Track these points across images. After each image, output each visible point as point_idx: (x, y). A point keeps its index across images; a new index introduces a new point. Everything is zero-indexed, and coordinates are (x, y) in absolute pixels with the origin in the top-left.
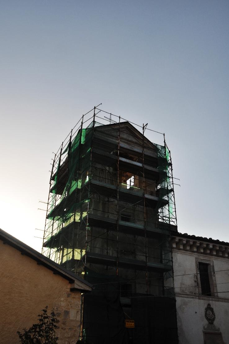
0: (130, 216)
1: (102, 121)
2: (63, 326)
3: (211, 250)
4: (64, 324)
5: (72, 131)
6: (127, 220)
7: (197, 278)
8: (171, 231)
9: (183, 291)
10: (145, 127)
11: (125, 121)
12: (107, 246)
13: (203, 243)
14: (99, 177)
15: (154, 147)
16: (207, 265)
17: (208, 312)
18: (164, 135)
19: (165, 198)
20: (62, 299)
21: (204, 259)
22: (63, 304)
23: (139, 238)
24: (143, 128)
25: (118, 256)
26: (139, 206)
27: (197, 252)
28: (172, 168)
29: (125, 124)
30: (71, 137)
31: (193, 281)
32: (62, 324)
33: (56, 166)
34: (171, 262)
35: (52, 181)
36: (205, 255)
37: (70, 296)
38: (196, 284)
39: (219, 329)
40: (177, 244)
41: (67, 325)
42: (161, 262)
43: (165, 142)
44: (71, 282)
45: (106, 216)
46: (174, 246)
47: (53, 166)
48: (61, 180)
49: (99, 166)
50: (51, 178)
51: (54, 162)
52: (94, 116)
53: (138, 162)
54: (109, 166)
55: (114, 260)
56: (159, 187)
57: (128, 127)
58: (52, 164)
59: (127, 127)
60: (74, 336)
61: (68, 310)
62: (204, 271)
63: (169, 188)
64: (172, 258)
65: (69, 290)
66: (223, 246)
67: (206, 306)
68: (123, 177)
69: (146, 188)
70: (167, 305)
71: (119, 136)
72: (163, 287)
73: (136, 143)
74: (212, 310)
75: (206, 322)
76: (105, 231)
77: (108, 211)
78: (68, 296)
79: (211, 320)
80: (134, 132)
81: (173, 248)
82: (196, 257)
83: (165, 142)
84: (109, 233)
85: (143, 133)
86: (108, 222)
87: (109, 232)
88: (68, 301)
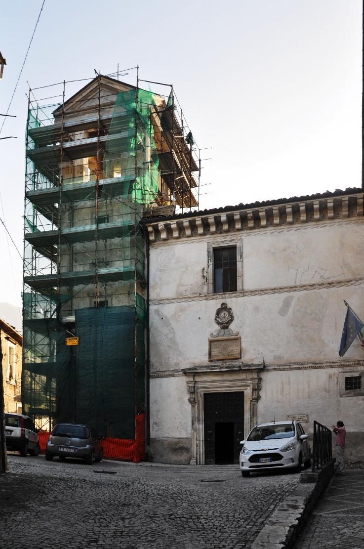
21: (222, 240)
39: (238, 333)
43: (64, 92)
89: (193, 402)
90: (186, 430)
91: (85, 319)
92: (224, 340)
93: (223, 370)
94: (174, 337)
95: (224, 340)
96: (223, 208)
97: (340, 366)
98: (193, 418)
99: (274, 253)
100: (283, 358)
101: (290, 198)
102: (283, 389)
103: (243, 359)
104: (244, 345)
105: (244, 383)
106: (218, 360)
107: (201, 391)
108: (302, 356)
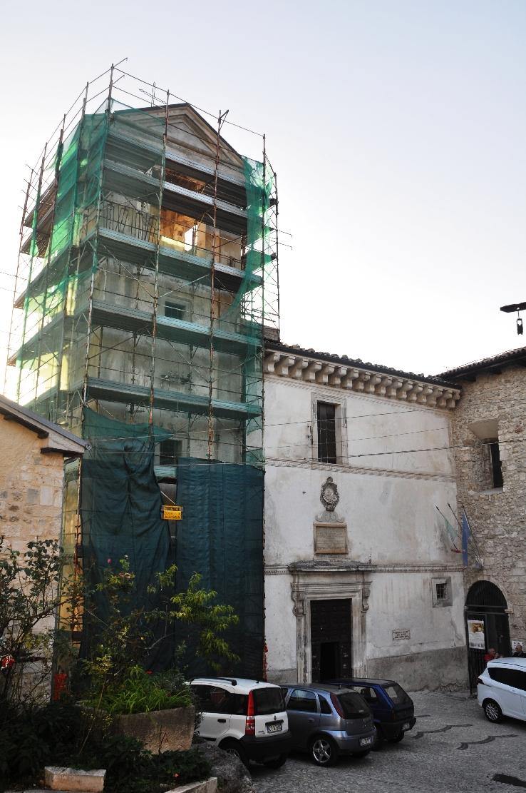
0: (183, 307)
1: (131, 98)
2: (26, 516)
3: (343, 378)
4: (29, 513)
5: (64, 119)
6: (179, 316)
7: (311, 432)
8: (265, 339)
9: (283, 454)
10: (223, 118)
11: (183, 102)
12: (134, 367)
13: (286, 357)
14: (118, 222)
15: (242, 165)
16: (334, 406)
17: (326, 492)
18: (264, 138)
19: (258, 272)
20: (24, 468)
21: (329, 395)
22: (25, 477)
23: (201, 351)
24: (220, 120)
25: (152, 386)
26: (204, 286)
27: (317, 381)
28: (277, 210)
29: (182, 109)
30: (62, 132)
31: (304, 437)
32: (25, 514)
33: (34, 194)
34: (261, 401)
35: (25, 228)
36: (330, 388)
37: (41, 462)
38: (310, 442)
39: (343, 519)
40: (277, 365)
41: (34, 514)
42: (243, 400)
43: (264, 153)
44: (43, 435)
45: (133, 306)
46: (271, 368)
47: (28, 196)
48: (41, 225)
49: (120, 199)
50: (22, 223)
51: (30, 185)
52: (111, 86)
53: (207, 193)
54: (142, 201)
55: (145, 395)
56: (247, 249)
57: (187, 116)
58: (26, 192)
59: (186, 115)
60: (50, 534)
61: (36, 489)
62: (327, 416)
63: (268, 253)
64: (263, 392)
65: (37, 451)
66: (368, 372)
67: (324, 481)
68: (176, 226)
69: (220, 251)
70: (250, 480)
71: (166, 134)
72: (244, 447)
73: (203, 153)
74: (334, 487)
75: (321, 508)
76: (131, 335)
77: (137, 294)
78: (37, 462)
79: (330, 504)
80: (201, 128)
81: (268, 373)
82: (312, 391)
83: (264, 153)
84: (137, 340)
85: (219, 130)
86: (133, 318)
87: (138, 336)
88: (36, 472)
89: (297, 612)
90: (291, 658)
91: (194, 477)
92: (330, 530)
93: (341, 570)
94: (274, 513)
95: (330, 530)
96: (340, 357)
97: (432, 571)
98: (299, 636)
99: (374, 425)
100: (386, 557)
101: (376, 366)
102: (387, 596)
103: (349, 556)
104: (350, 536)
105: (352, 588)
106: (324, 554)
107: (308, 598)
108: (401, 557)
